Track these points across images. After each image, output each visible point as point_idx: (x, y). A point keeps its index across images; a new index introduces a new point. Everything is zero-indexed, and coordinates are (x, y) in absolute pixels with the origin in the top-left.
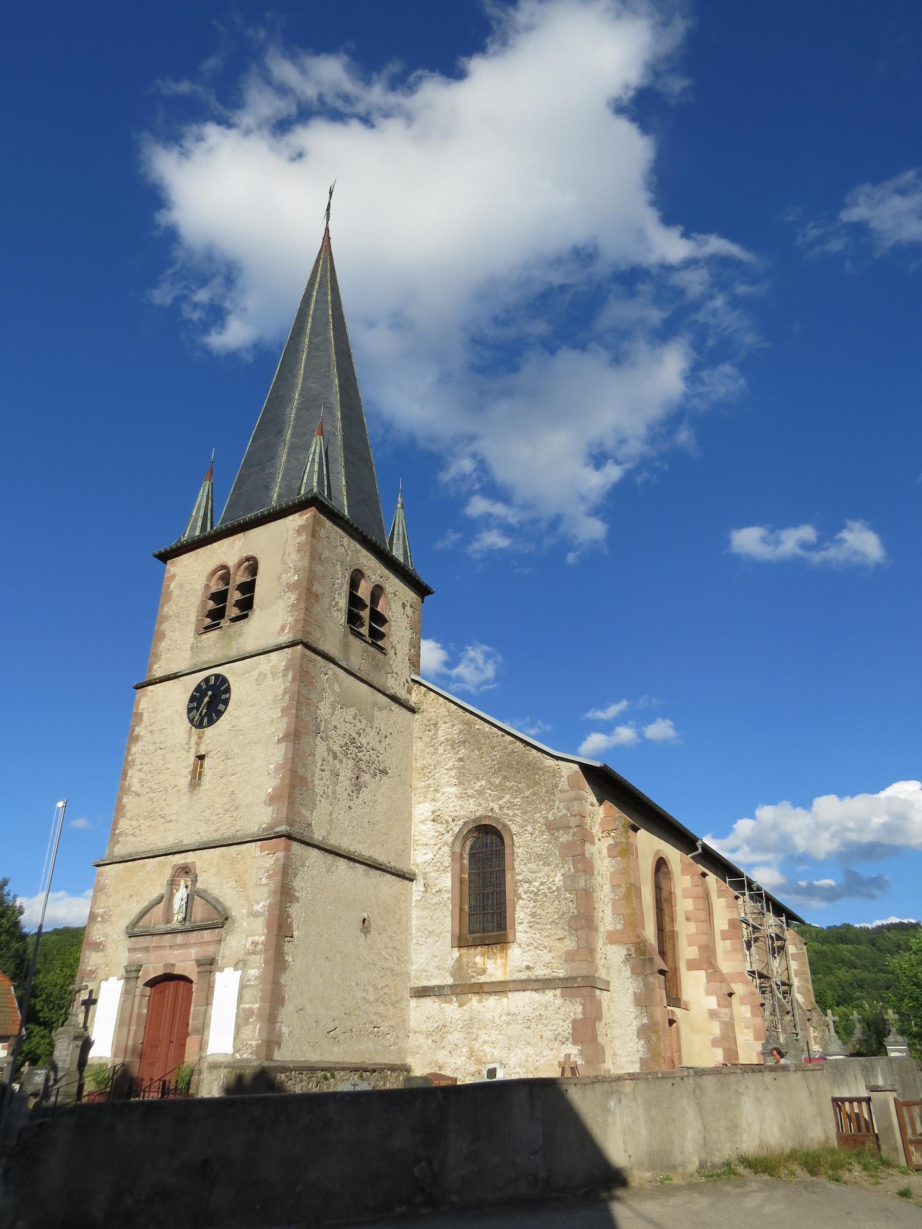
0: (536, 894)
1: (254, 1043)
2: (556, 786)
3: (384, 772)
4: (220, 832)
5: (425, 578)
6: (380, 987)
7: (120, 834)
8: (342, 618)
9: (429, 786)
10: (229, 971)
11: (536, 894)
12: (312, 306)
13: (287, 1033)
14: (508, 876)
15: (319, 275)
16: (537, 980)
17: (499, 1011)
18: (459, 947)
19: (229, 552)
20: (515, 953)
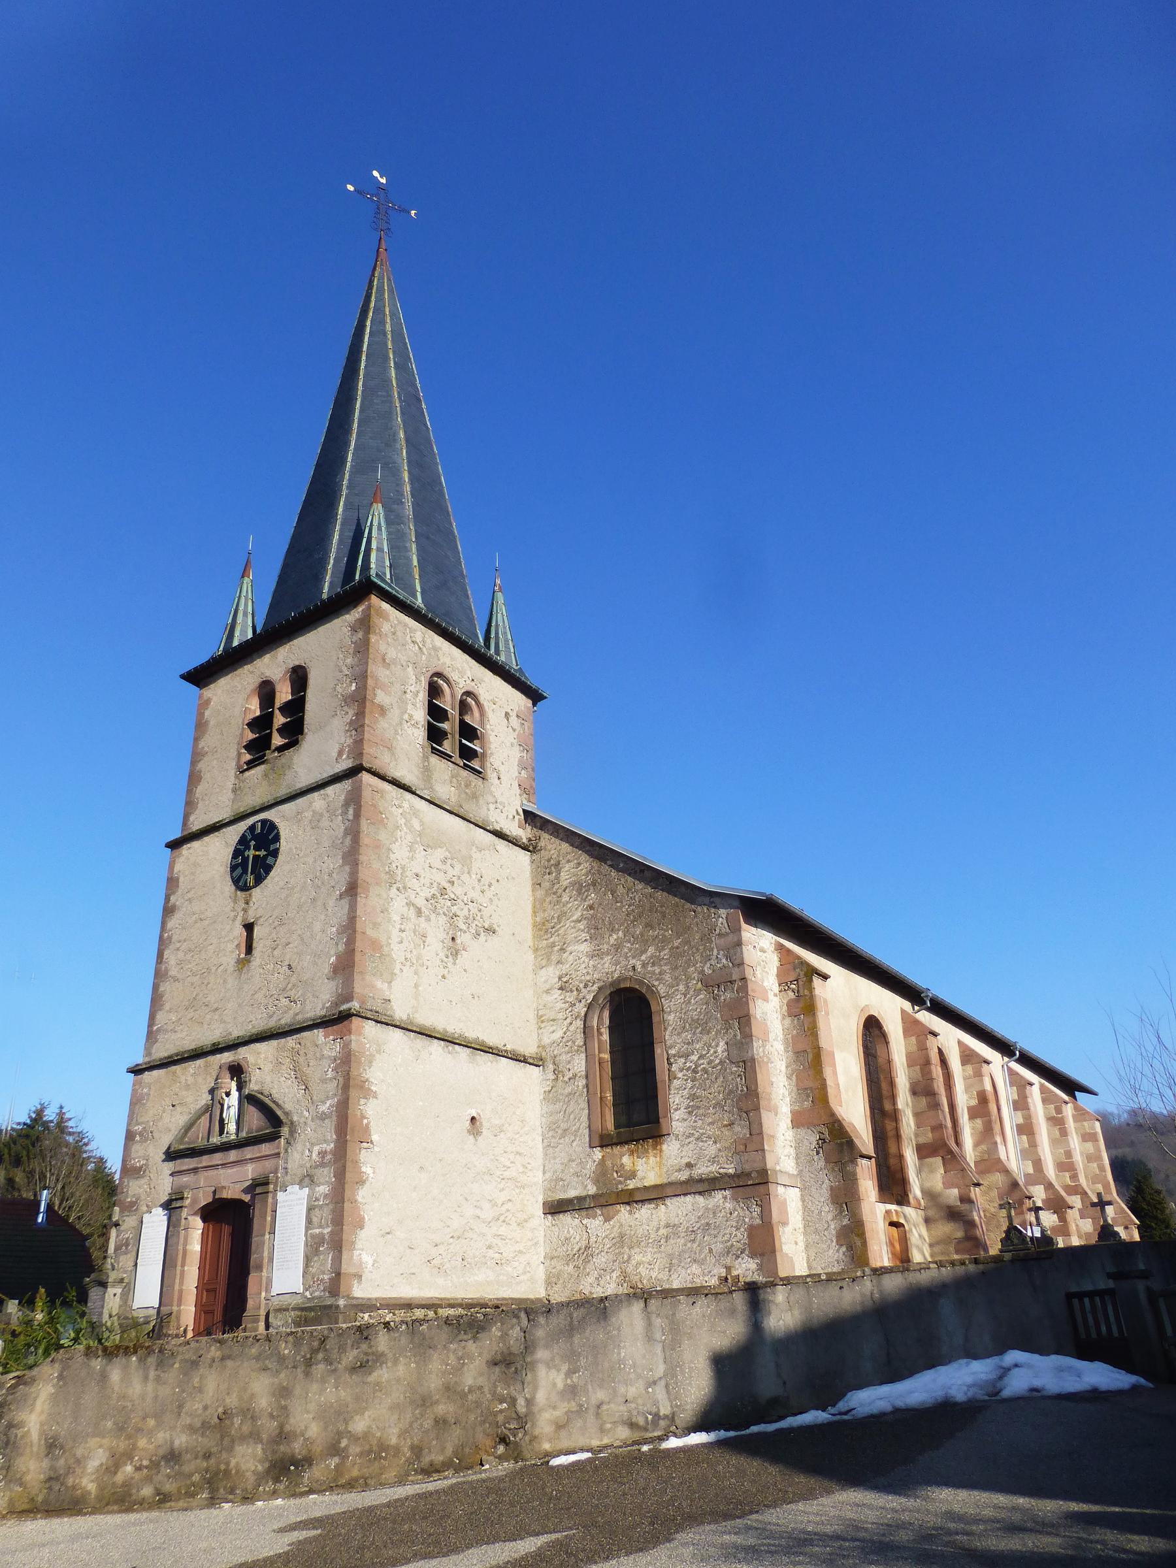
0: (695, 1071)
1: (326, 1277)
2: (712, 930)
3: (491, 931)
4: (275, 1018)
5: (533, 681)
6: (500, 1202)
7: (159, 1030)
8: (421, 734)
9: (553, 945)
10: (294, 1189)
11: (695, 1071)
12: (366, 339)
13: (370, 1262)
14: (658, 1051)
15: (373, 298)
16: (701, 1180)
17: (655, 1223)
18: (602, 1146)
19: (274, 666)
20: (670, 1148)
